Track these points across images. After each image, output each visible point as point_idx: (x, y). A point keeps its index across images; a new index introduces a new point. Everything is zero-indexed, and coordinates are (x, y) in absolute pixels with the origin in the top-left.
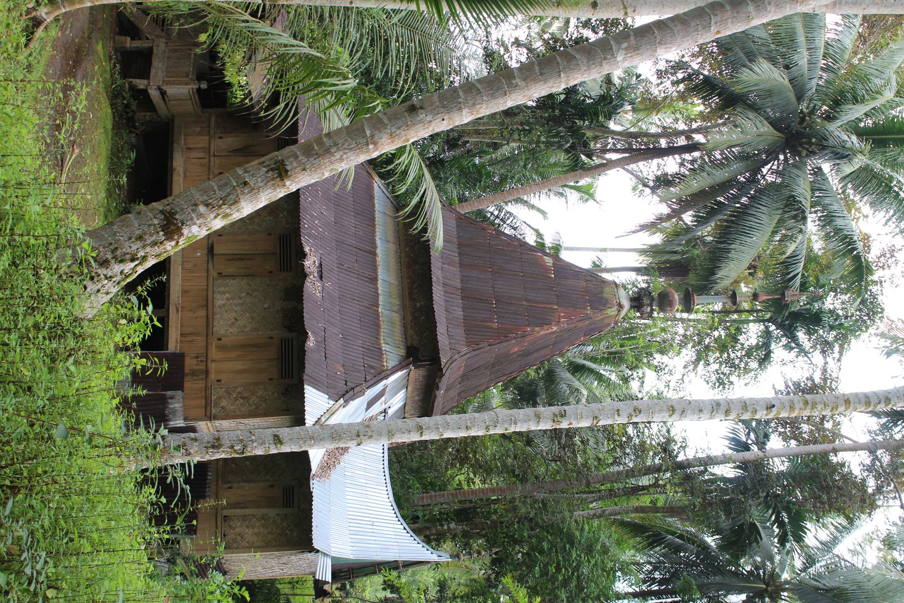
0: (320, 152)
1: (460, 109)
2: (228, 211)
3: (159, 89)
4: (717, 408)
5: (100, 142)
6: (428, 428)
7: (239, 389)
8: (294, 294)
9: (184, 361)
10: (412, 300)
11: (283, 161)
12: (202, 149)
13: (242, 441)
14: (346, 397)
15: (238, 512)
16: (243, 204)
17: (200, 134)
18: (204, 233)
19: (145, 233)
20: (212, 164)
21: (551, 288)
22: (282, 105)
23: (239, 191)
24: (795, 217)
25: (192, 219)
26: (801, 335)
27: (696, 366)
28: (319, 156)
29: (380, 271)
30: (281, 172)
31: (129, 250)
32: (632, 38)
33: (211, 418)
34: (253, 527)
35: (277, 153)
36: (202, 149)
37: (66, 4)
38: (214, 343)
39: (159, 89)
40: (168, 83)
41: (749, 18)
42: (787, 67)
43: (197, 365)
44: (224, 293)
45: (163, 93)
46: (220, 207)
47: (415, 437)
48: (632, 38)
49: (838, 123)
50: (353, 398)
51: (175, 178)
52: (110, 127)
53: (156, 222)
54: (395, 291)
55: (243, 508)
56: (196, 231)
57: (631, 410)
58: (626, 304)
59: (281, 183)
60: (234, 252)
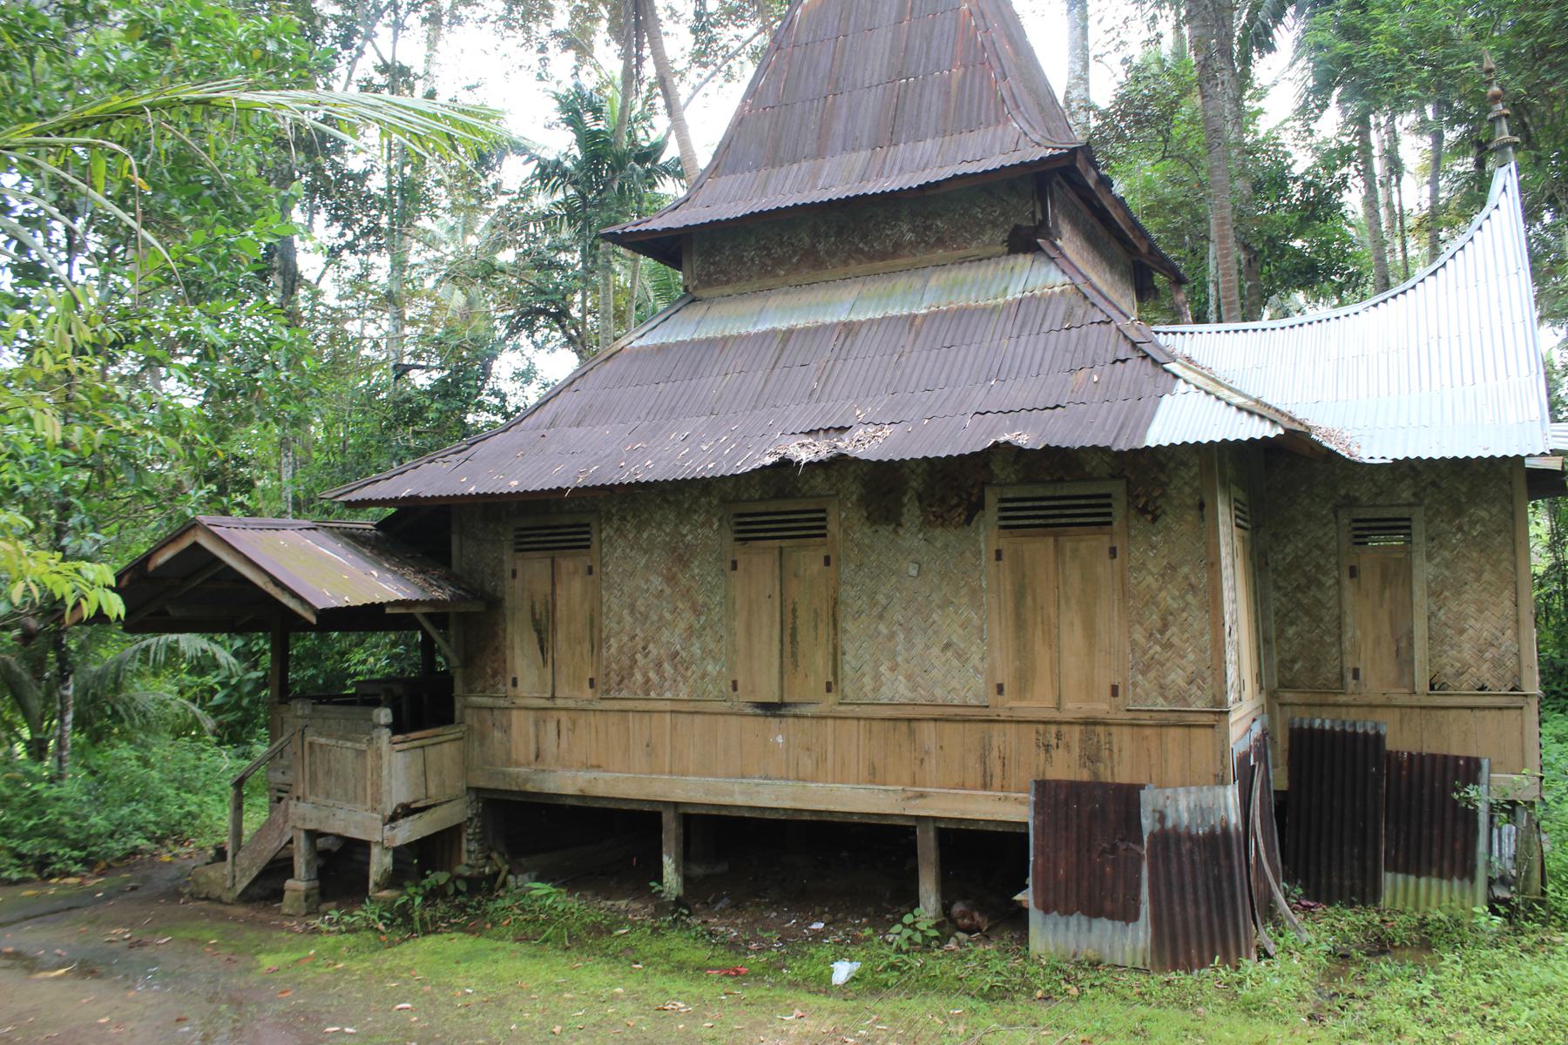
3: (394, 818)
7: (1139, 635)
8: (886, 490)
9: (1058, 783)
10: (897, 249)
14: (1160, 358)
17: (506, 730)
20: (571, 704)
33: (1220, 712)
38: (1010, 704)
39: (394, 818)
40: (377, 799)
43: (1068, 746)
44: (877, 677)
51: (600, 790)
54: (876, 287)
55: (1411, 645)
60: (776, 663)
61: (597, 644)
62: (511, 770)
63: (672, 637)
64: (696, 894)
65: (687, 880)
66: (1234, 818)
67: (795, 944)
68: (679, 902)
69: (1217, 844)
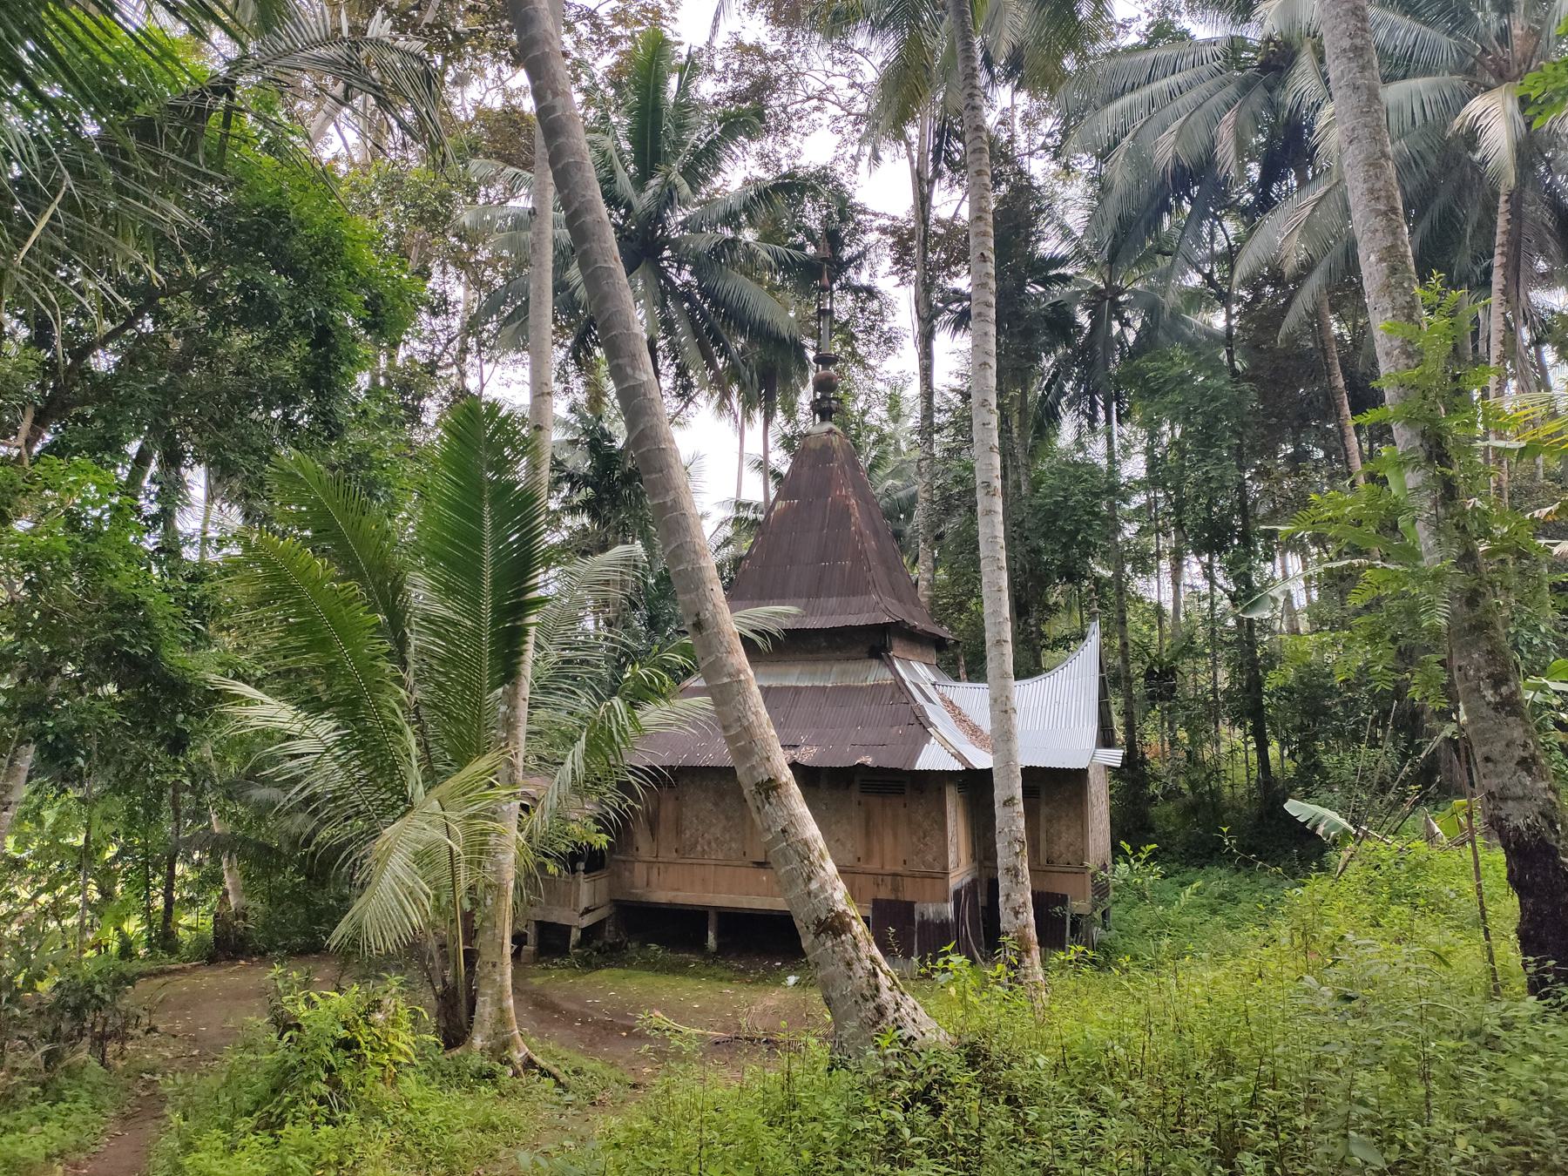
1: (700, 569)
15: (1043, 846)
16: (808, 835)
17: (632, 872)
18: (841, 884)
22: (631, 778)
24: (731, 251)
26: (847, 253)
27: (872, 368)
29: (787, 683)
30: (770, 787)
31: (865, 979)
32: (620, 361)
33: (945, 873)
34: (1060, 832)
38: (863, 866)
40: (576, 904)
41: (600, 222)
45: (587, 911)
46: (811, 863)
47: (1009, 649)
48: (620, 361)
49: (635, 201)
50: (927, 718)
52: (621, 972)
53: (829, 944)
56: (839, 894)
57: (984, 410)
58: (828, 426)
61: (679, 832)
62: (1346, 824)
63: (717, 831)
64: (723, 950)
65: (719, 945)
66: (951, 916)
67: (770, 970)
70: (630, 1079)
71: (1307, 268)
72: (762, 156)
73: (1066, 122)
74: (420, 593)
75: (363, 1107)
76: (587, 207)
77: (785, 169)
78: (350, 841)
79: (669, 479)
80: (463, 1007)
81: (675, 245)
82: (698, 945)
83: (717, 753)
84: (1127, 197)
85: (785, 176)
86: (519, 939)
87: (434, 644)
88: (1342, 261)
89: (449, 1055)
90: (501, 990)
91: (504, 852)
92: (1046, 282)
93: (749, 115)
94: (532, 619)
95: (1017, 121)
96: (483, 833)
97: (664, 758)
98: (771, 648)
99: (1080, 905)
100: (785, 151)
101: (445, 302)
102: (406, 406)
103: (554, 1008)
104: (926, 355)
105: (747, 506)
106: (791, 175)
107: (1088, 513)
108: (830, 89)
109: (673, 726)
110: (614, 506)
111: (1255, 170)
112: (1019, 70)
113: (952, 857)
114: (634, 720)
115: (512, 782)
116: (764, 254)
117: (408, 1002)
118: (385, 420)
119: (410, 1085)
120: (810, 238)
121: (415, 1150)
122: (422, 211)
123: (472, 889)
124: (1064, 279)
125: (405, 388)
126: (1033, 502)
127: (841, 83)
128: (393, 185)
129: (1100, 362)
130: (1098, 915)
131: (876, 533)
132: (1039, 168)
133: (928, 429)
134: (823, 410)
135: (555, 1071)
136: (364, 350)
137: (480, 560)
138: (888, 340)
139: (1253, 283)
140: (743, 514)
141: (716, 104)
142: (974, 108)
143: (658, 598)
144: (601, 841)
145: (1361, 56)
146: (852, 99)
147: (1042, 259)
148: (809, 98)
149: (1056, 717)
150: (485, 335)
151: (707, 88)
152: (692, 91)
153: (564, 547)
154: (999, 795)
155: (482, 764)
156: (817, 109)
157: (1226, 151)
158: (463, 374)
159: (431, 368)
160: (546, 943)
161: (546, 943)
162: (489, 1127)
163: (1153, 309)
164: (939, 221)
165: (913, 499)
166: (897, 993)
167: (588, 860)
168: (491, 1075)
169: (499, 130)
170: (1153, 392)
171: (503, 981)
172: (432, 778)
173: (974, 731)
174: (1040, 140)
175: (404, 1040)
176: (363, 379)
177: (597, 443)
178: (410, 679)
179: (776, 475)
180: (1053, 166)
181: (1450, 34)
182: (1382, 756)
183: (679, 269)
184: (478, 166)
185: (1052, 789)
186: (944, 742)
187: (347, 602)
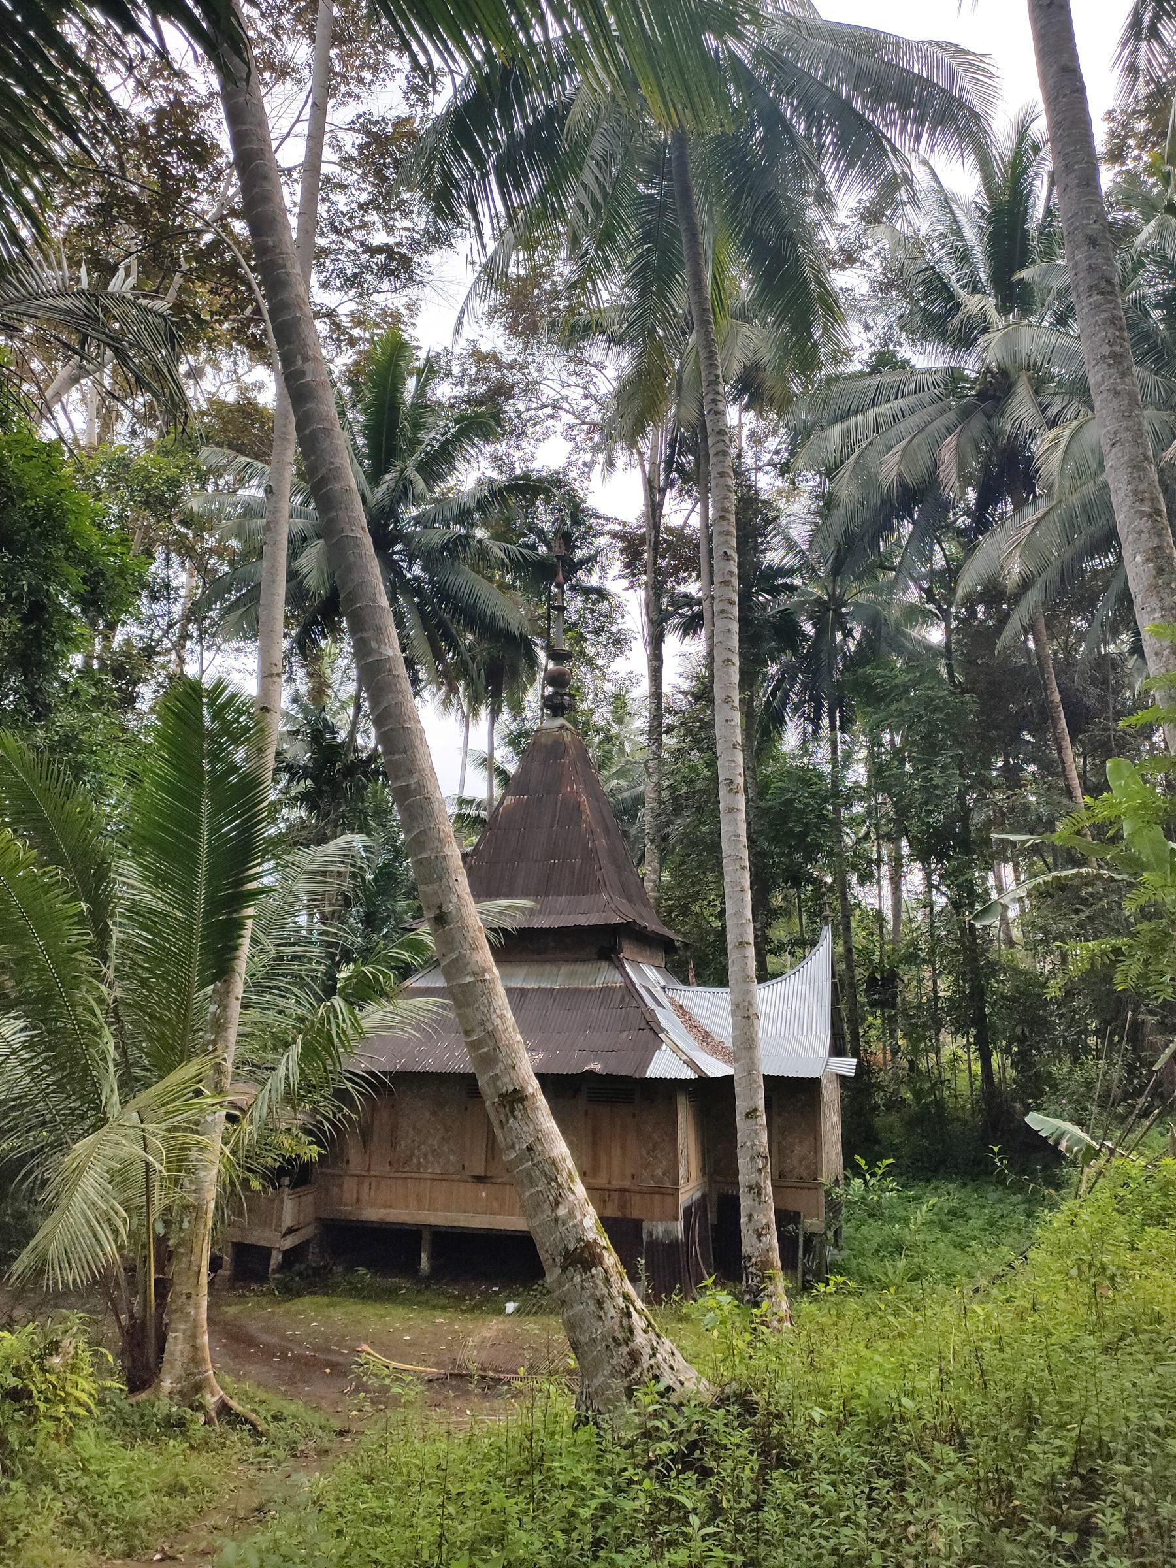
0: (492, 1045)
1: (444, 857)
2: (565, 1174)
4: (656, 642)
5: (346, 1313)
6: (741, 935)
7: (644, 1153)
11: (501, 1096)
12: (360, 1184)
13: (752, 1159)
17: (341, 1187)
18: (591, 1210)
19: (593, 1295)
21: (540, 800)
22: (349, 1085)
23: (540, 1158)
24: (464, 547)
25: (575, 1226)
26: (578, 554)
27: (598, 667)
28: (496, 1047)
30: (515, 1099)
31: (617, 1320)
32: (365, 635)
35: (488, 1103)
36: (360, 1184)
37: (202, 1369)
40: (279, 1225)
41: (348, 491)
42: (305, 539)
45: (290, 1231)
46: (560, 1186)
48: (365, 635)
52: (325, 1299)
53: (578, 1279)
54: (535, 969)
58: (560, 721)
59: (531, 1100)
61: (394, 1143)
63: (434, 1142)
65: (433, 1268)
66: (681, 1235)
67: (487, 1298)
68: (429, 1278)
69: (672, 1247)
70: (337, 1425)
71: (1026, 584)
72: (496, 458)
73: (794, 439)
74: (129, 880)
75: (31, 1471)
76: (335, 474)
77: (518, 472)
78: (33, 1154)
79: (413, 760)
80: (151, 1350)
81: (407, 539)
82: (410, 1268)
83: (458, 1060)
84: (851, 513)
85: (518, 478)
86: (215, 1264)
87: (139, 936)
88: (1057, 578)
89: (133, 1400)
90: (196, 1326)
91: (205, 1168)
92: (774, 591)
93: (485, 417)
94: (250, 911)
95: (744, 439)
96: (183, 1147)
97: (383, 1063)
98: (514, 945)
99: (813, 1223)
100: (518, 454)
101: (167, 586)
102: (119, 689)
103: (251, 1342)
104: (656, 657)
105: (470, 802)
106: (526, 476)
107: (817, 817)
108: (565, 398)
109: (399, 1028)
110: (334, 798)
111: (972, 495)
112: (753, 388)
113: (682, 1171)
114: (356, 1021)
115: (219, 1090)
116: (496, 550)
117: (90, 1343)
118: (97, 702)
119: (87, 1441)
120: (543, 539)
121: (89, 1522)
122: (149, 496)
123: (168, 1210)
124: (792, 588)
125: (118, 671)
126: (762, 804)
127: (575, 394)
128: (121, 466)
129: (825, 670)
130: (830, 1234)
131: (607, 831)
132: (766, 482)
133: (656, 730)
134: (556, 706)
135: (253, 1416)
136: (79, 627)
137: (196, 847)
138: (617, 642)
139: (970, 603)
140: (466, 811)
141: (452, 406)
142: (717, 413)
143: (378, 894)
144: (312, 1152)
145: (1121, 363)
146: (587, 409)
147: (770, 567)
148: (544, 406)
149: (791, 1022)
150: (207, 622)
151: (443, 391)
152: (429, 393)
153: (280, 840)
154: (741, 1106)
155: (189, 1070)
156: (551, 417)
157: (949, 473)
158: (182, 661)
159: (150, 651)
160: (243, 1267)
161: (243, 1267)
162: (176, 1489)
163: (874, 623)
164: (668, 529)
165: (639, 800)
166: (652, 1336)
167: (296, 1174)
168: (181, 1423)
169: (232, 421)
170: (880, 699)
171: (197, 1314)
172: (129, 1085)
173: (705, 1038)
174: (766, 457)
175: (84, 1388)
176: (77, 660)
177: (319, 734)
178: (111, 975)
179: (501, 773)
180: (779, 483)
181: (1156, 374)
182: (1104, 1070)
183: (410, 563)
184: (208, 455)
185: (791, 1096)
186: (676, 1049)
187: (46, 889)
